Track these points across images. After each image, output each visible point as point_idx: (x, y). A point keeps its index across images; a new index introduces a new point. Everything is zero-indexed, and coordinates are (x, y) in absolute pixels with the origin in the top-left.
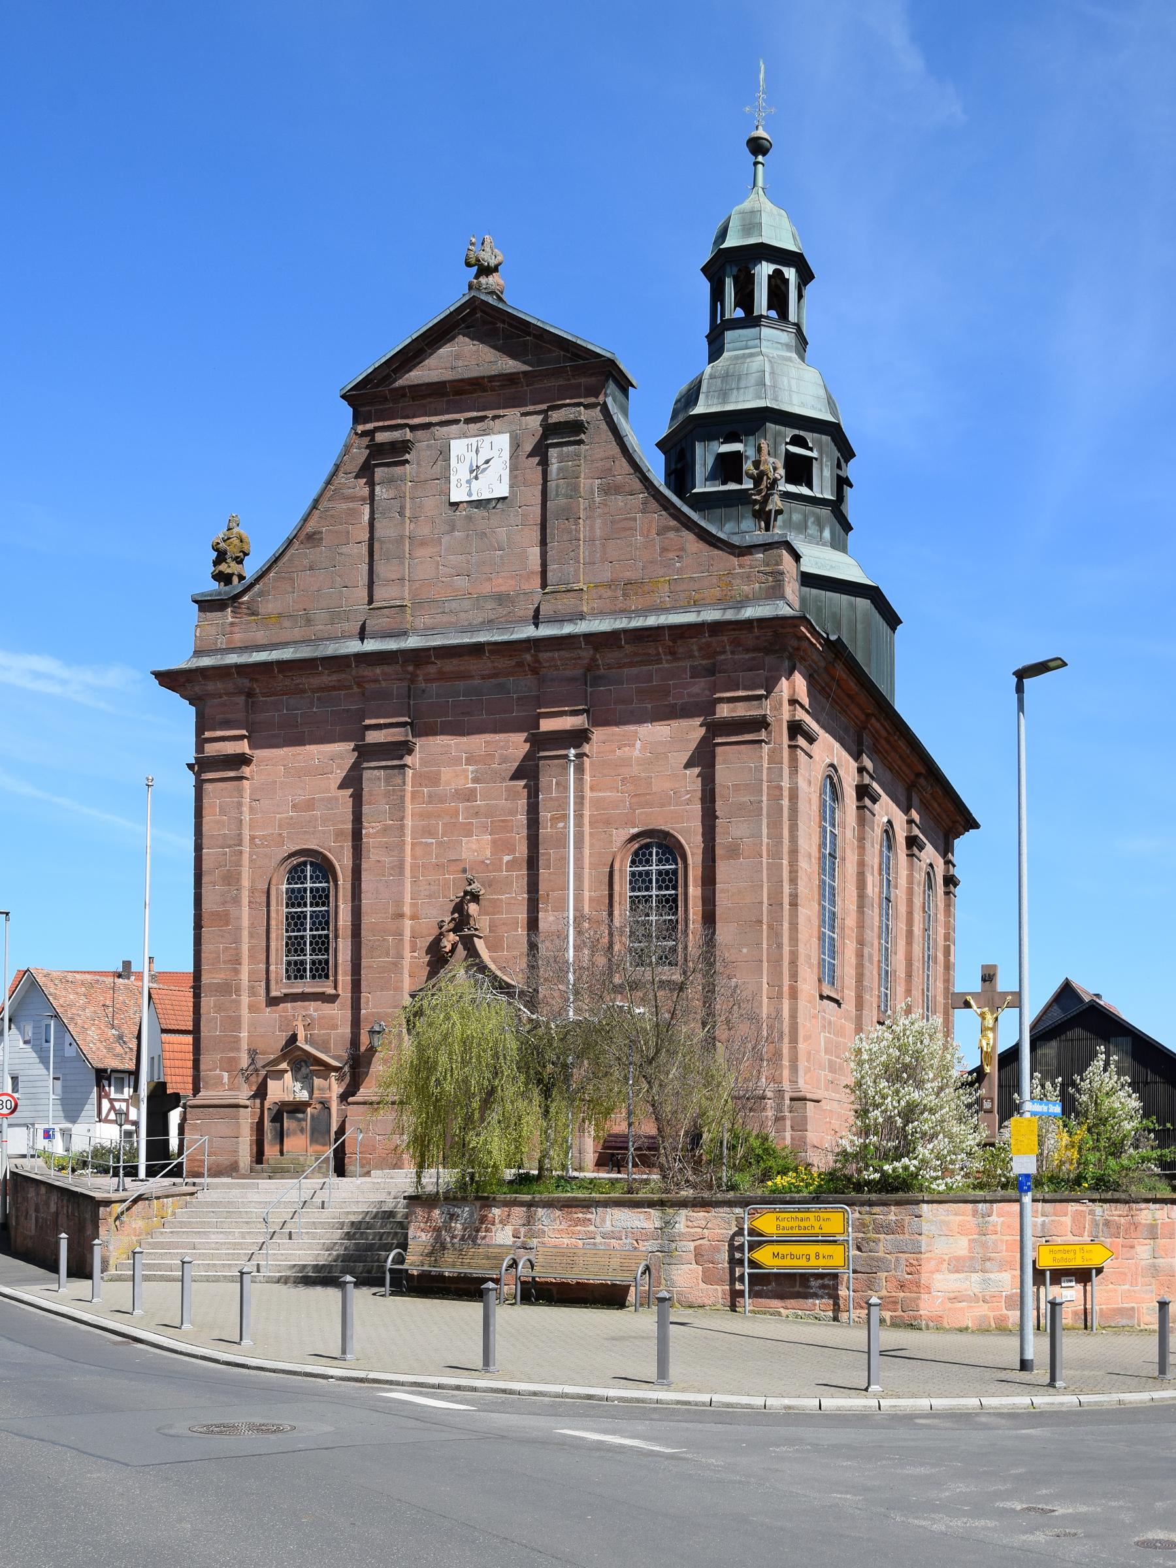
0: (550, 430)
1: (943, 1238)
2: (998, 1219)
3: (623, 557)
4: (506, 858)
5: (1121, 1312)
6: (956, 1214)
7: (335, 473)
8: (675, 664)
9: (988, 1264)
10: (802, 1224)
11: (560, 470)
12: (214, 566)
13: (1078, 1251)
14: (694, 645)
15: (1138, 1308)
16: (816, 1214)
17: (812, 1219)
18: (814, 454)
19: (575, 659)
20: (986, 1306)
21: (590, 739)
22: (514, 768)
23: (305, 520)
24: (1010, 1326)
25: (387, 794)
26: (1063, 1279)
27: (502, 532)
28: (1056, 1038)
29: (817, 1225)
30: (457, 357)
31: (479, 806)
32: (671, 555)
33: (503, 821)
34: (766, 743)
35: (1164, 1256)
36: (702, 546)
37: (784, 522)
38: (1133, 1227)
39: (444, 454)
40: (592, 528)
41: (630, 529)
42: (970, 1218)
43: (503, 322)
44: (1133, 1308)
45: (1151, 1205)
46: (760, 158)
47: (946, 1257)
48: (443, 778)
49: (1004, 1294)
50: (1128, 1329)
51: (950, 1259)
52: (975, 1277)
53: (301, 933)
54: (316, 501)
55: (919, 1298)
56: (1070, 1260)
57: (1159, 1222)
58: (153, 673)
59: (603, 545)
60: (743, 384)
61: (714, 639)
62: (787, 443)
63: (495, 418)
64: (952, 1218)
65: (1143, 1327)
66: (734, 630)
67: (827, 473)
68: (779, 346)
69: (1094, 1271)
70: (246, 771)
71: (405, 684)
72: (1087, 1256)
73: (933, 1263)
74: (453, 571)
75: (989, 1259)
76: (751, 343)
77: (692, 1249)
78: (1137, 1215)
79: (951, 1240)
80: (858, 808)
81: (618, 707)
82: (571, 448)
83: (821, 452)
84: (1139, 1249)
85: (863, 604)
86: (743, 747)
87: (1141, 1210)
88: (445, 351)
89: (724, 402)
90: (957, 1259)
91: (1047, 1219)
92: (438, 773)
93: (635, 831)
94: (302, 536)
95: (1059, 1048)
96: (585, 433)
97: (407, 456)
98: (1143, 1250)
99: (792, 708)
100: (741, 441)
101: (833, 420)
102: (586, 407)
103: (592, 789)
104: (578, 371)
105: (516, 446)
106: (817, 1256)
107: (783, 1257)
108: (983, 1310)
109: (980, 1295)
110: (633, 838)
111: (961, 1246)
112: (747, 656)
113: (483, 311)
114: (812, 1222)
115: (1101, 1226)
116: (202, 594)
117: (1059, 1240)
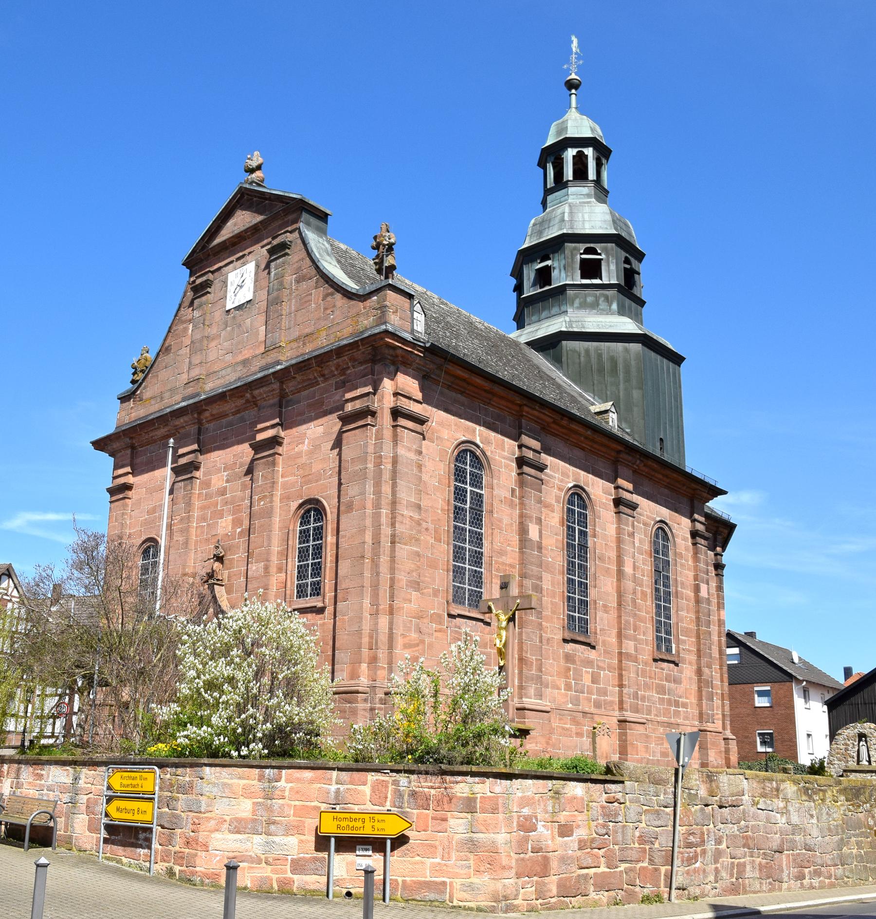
0: (271, 252)
1: (225, 800)
2: (285, 785)
3: (304, 320)
4: (239, 530)
5: (428, 885)
7: (179, 310)
8: (327, 383)
11: (275, 274)
13: (367, 820)
14: (332, 364)
15: (451, 883)
19: (272, 391)
20: (269, 868)
21: (282, 443)
22: (245, 470)
23: (165, 340)
24: (295, 890)
25: (184, 497)
26: (358, 847)
30: (235, 225)
34: (373, 426)
35: (485, 831)
36: (345, 300)
37: (580, 304)
38: (446, 799)
39: (225, 283)
42: (255, 782)
43: (255, 197)
44: (444, 884)
45: (469, 779)
46: (573, 91)
47: (227, 818)
48: (213, 482)
49: (289, 858)
50: (437, 904)
51: (231, 819)
52: (257, 839)
54: (170, 328)
55: (196, 855)
56: (357, 828)
57: (478, 796)
59: (295, 315)
60: (551, 225)
61: (340, 360)
62: (581, 254)
63: (250, 253)
64: (236, 781)
65: (455, 903)
67: (613, 267)
68: (582, 196)
69: (389, 843)
70: (129, 493)
71: (197, 426)
73: (213, 823)
75: (274, 823)
76: (562, 199)
77: (85, 801)
78: (451, 788)
79: (233, 801)
83: (607, 255)
84: (452, 822)
85: (636, 347)
86: (357, 431)
87: (457, 783)
88: (230, 224)
89: (540, 238)
90: (239, 820)
91: (342, 788)
92: (210, 480)
93: (301, 501)
94: (163, 349)
96: (289, 249)
98: (458, 824)
99: (395, 399)
100: (549, 259)
101: (615, 232)
102: (291, 232)
103: (282, 477)
104: (287, 212)
105: (257, 266)
108: (266, 872)
109: (263, 857)
110: (301, 506)
111: (245, 808)
112: (362, 368)
113: (248, 194)
115: (406, 797)
116: (122, 394)
117: (356, 808)
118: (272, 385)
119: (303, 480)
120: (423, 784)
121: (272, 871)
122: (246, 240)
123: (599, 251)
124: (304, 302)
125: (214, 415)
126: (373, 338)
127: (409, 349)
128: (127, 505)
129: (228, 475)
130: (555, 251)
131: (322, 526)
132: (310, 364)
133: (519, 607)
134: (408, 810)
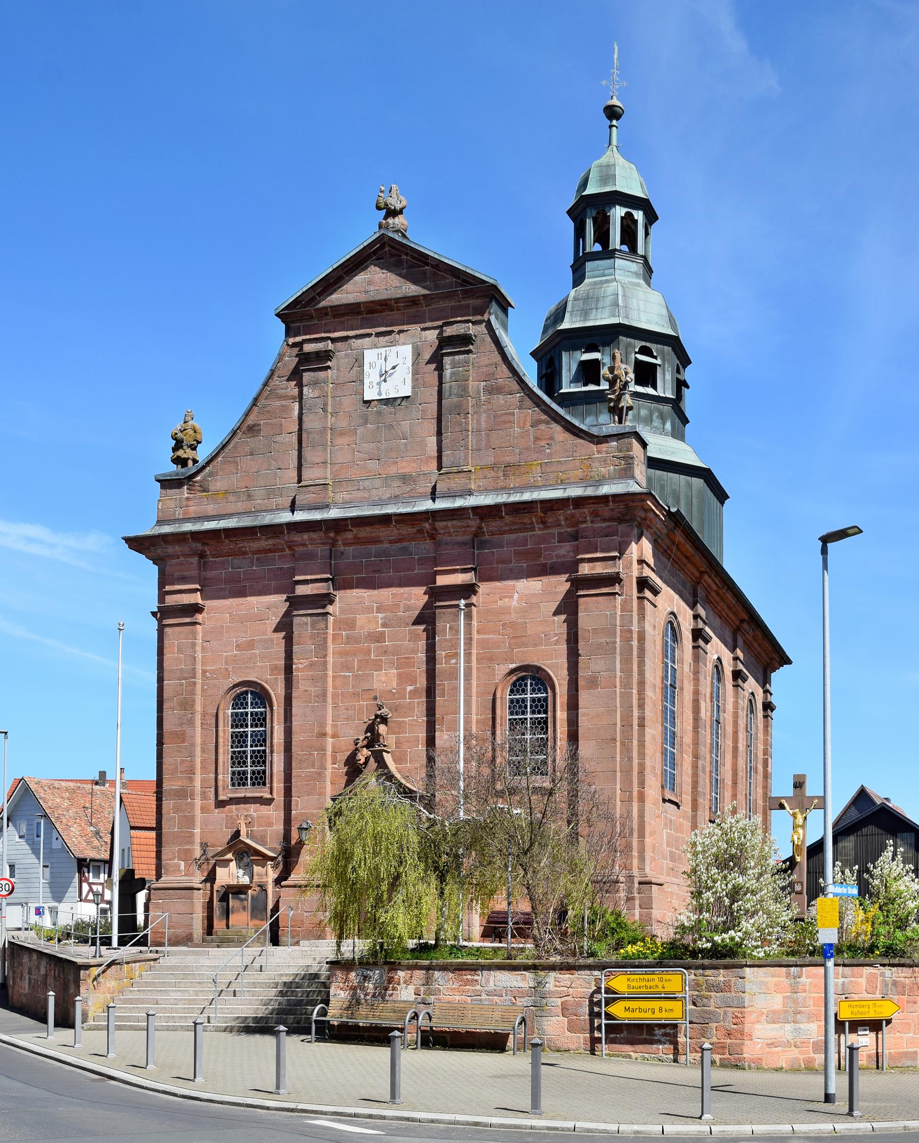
0: (444, 342)
1: (762, 995)
3: (503, 445)
4: (409, 688)
5: (906, 1055)
6: (772, 976)
8: (545, 532)
9: (799, 1016)
10: (649, 984)
11: (453, 374)
12: (173, 452)
13: (871, 1006)
14: (561, 516)
16: (660, 976)
17: (657, 980)
18: (658, 362)
20: (797, 1050)
21: (477, 592)
22: (415, 616)
23: (247, 414)
24: (816, 1067)
26: (859, 1028)
27: (405, 425)
28: (853, 834)
29: (660, 984)
31: (387, 646)
32: (542, 443)
33: (406, 658)
34: (619, 595)
37: (634, 416)
40: (479, 421)
41: (509, 422)
42: (784, 979)
43: (407, 255)
46: (614, 122)
47: (765, 1011)
49: (812, 1040)
50: (912, 1068)
52: (788, 1027)
53: (243, 749)
55: (743, 1044)
58: (123, 538)
59: (488, 435)
60: (600, 305)
61: (577, 511)
62: (636, 353)
63: (400, 332)
64: (769, 979)
66: (593, 503)
67: (668, 377)
68: (630, 274)
70: (199, 617)
72: (878, 1010)
73: (754, 1016)
74: (366, 456)
75: (800, 1013)
76: (607, 272)
77: (560, 1004)
80: (694, 647)
81: (500, 566)
82: (462, 357)
83: (663, 360)
85: (698, 482)
89: (585, 320)
92: (354, 620)
93: (513, 666)
94: (244, 428)
95: (856, 842)
97: (329, 363)
99: (640, 567)
100: (599, 351)
101: (673, 334)
102: (474, 323)
103: (478, 632)
105: (417, 354)
106: (661, 1010)
107: (633, 1011)
108: (794, 1053)
109: (792, 1041)
110: (512, 672)
111: (777, 1002)
112: (604, 525)
114: (657, 982)
115: (890, 986)
116: (163, 475)
118: (468, 521)
119: (513, 641)
120: (900, 975)
121: (799, 1052)
122: (392, 310)
123: (655, 354)
124: (499, 422)
125: (359, 538)
126: (631, 497)
127: (658, 513)
128: (194, 634)
129: (385, 618)
130: (607, 344)
131: (546, 699)
132: (533, 508)
133: (816, 807)
134: (891, 996)
